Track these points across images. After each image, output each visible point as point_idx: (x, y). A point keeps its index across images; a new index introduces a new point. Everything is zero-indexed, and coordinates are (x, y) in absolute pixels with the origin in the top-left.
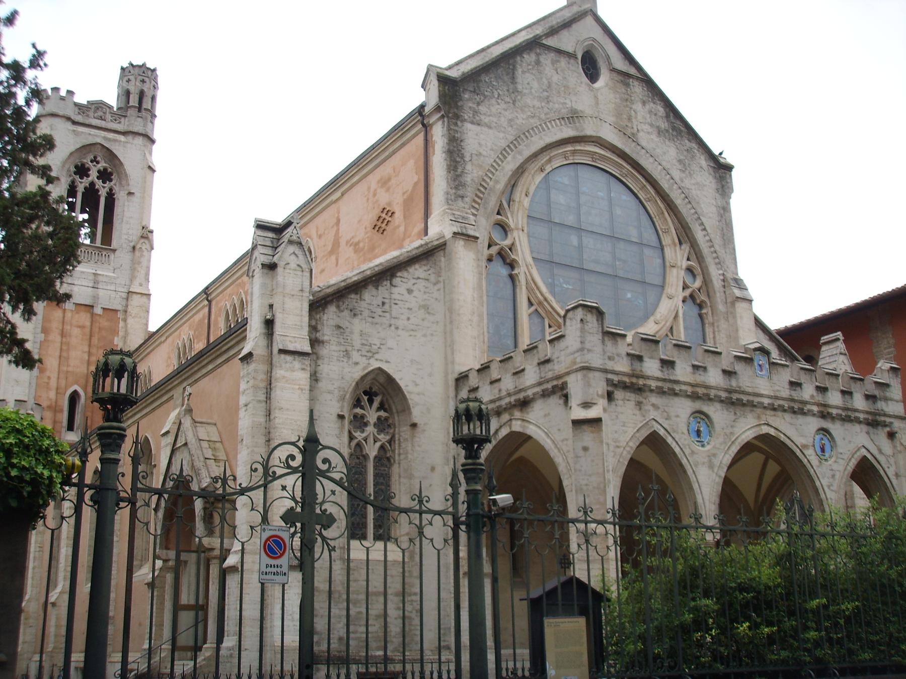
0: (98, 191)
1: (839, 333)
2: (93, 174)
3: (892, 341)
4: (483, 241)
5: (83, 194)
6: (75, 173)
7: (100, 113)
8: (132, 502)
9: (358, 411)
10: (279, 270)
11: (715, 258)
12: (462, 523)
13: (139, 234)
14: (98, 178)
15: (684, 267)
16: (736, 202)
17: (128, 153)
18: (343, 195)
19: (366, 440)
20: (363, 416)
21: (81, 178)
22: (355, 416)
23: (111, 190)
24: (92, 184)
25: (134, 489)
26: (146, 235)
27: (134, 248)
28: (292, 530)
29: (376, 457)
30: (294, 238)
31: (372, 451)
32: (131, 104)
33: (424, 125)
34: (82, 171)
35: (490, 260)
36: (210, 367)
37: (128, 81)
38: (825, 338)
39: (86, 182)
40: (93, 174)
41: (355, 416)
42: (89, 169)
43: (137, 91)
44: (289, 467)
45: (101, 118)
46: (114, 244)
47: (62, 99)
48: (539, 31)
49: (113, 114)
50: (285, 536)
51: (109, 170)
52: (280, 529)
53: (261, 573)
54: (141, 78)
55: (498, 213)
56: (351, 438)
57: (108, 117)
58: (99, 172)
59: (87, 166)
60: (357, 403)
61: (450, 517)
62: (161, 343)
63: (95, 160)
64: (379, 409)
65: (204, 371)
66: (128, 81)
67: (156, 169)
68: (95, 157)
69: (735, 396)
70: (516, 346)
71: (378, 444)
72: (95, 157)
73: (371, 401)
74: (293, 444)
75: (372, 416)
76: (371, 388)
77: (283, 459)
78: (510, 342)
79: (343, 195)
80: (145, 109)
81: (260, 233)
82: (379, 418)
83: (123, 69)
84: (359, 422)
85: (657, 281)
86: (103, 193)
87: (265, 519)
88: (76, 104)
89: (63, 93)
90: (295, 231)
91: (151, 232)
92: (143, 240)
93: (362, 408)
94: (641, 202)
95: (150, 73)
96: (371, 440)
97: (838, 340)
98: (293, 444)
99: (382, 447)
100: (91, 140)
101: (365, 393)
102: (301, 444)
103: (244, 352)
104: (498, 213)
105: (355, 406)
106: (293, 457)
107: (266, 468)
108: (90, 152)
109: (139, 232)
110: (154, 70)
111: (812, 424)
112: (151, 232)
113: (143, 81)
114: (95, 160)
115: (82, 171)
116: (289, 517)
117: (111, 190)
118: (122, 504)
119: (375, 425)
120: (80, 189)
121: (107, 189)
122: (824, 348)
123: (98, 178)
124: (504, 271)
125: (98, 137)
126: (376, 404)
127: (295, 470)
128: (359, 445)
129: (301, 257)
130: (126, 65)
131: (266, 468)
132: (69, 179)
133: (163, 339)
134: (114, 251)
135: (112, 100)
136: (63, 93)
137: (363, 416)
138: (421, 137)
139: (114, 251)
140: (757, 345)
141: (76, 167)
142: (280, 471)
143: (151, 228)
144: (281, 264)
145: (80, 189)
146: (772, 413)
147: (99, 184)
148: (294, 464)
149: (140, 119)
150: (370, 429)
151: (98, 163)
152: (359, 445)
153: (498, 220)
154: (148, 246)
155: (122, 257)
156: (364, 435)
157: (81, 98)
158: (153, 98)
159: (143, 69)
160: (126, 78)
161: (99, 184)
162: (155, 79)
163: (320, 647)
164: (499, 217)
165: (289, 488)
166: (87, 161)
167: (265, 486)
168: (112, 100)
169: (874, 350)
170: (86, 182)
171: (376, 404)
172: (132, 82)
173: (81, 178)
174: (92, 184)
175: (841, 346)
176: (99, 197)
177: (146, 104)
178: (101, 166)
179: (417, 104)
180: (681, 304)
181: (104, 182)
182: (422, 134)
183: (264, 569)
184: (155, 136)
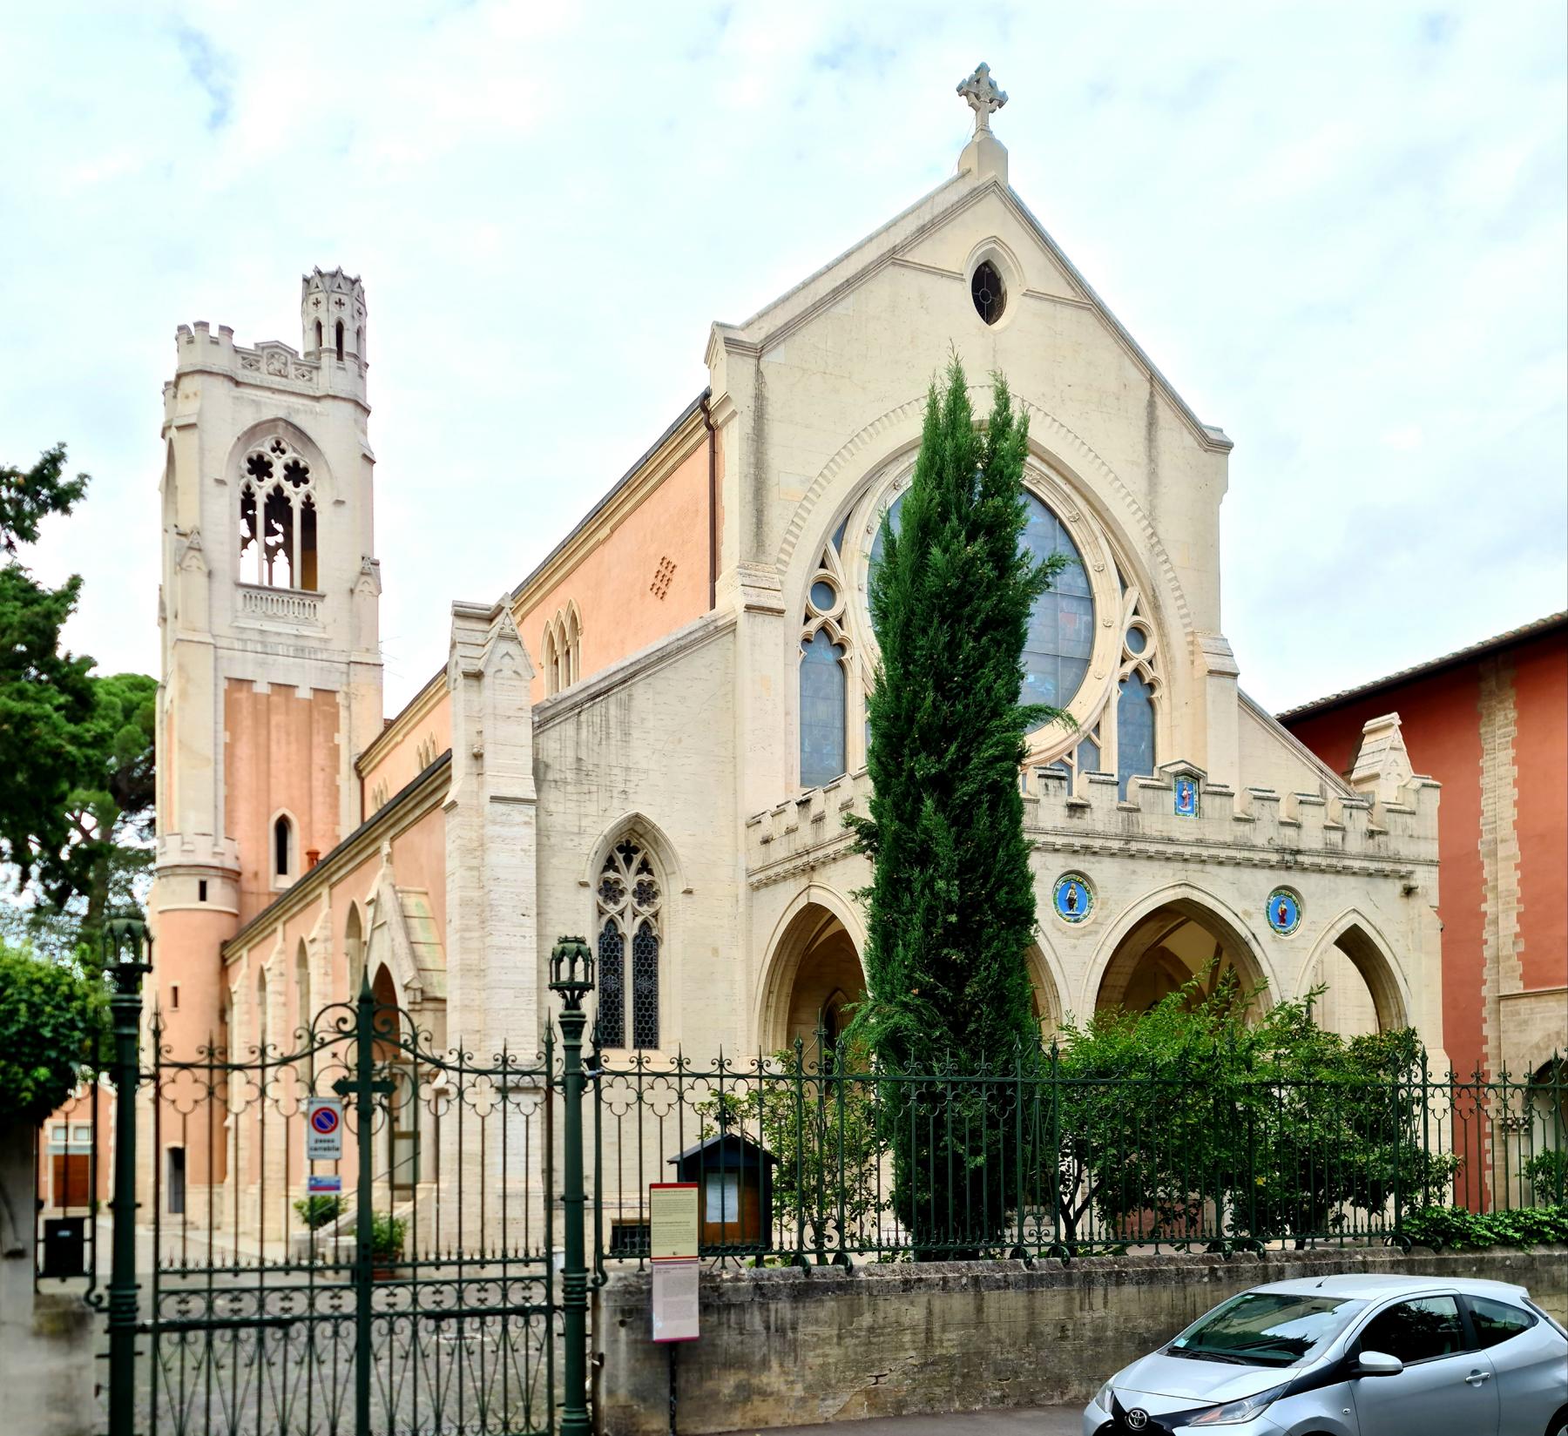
0: (288, 500)
1: (1395, 715)
2: (278, 471)
3: (1513, 715)
4: (795, 614)
5: (266, 505)
6: (251, 472)
7: (277, 365)
8: (155, 1077)
9: (611, 875)
10: (487, 680)
11: (1180, 608)
12: (558, 1084)
13: (358, 569)
14: (287, 478)
15: (1127, 626)
16: (1228, 509)
17: (326, 426)
18: (612, 532)
19: (621, 914)
20: (617, 882)
21: (260, 479)
22: (606, 882)
23: (308, 497)
24: (278, 489)
25: (158, 1065)
26: (370, 568)
27: (352, 591)
28: (345, 1101)
29: (636, 937)
30: (507, 630)
31: (629, 928)
32: (325, 345)
33: (710, 427)
34: (260, 467)
35: (807, 641)
36: (418, 812)
37: (317, 303)
38: (1370, 724)
39: (268, 485)
40: (278, 471)
41: (606, 882)
42: (270, 465)
43: (333, 323)
44: (340, 1031)
45: (280, 374)
46: (322, 586)
47: (215, 342)
48: (897, 237)
49: (299, 365)
50: (337, 1108)
51: (302, 464)
52: (331, 1101)
53: (311, 1149)
54: (336, 297)
55: (823, 565)
56: (601, 912)
57: (291, 370)
58: (287, 467)
59: (266, 459)
60: (610, 864)
61: (544, 1078)
62: (397, 744)
63: (277, 448)
64: (639, 872)
65: (411, 818)
66: (317, 303)
67: (376, 457)
68: (278, 443)
69: (1134, 846)
70: (844, 770)
71: (639, 920)
72: (278, 443)
73: (628, 861)
74: (344, 1005)
75: (629, 880)
76: (628, 842)
77: (333, 1023)
78: (835, 763)
79: (612, 532)
80: (349, 354)
81: (460, 623)
82: (640, 884)
83: (306, 281)
84: (610, 891)
85: (1079, 653)
86: (296, 505)
87: (312, 1089)
88: (236, 350)
89: (214, 331)
90: (507, 621)
91: (376, 564)
92: (364, 578)
93: (617, 870)
94: (1062, 524)
95: (346, 287)
96: (628, 914)
97: (1390, 726)
98: (344, 1005)
99: (645, 923)
100: (268, 414)
101: (620, 849)
102: (355, 1004)
103: (447, 801)
104: (823, 565)
105: (606, 869)
106: (344, 1021)
107: (312, 1037)
108: (269, 433)
109: (358, 565)
110: (355, 282)
111: (1266, 882)
112: (376, 564)
113: (340, 303)
114: (277, 448)
115: (260, 467)
116: (341, 1087)
117: (308, 497)
118: (143, 1081)
119: (634, 893)
120: (261, 500)
121: (302, 497)
122: (1366, 740)
123: (287, 478)
124: (830, 656)
125: (274, 406)
126: (635, 864)
127: (347, 1035)
128: (611, 921)
129: (519, 659)
130: (310, 274)
131: (312, 1037)
132: (243, 482)
133: (399, 738)
134: (323, 597)
135: (297, 339)
136: (214, 331)
137: (617, 882)
138: (705, 449)
139: (323, 597)
140: (1182, 767)
141: (250, 461)
142: (328, 1038)
143: (376, 557)
144: (489, 672)
145: (261, 500)
146: (1199, 867)
147: (288, 487)
148: (347, 1028)
149: (341, 373)
150: (628, 900)
151: (283, 452)
152: (611, 921)
153: (821, 577)
154: (372, 588)
155: (331, 610)
156: (618, 908)
157: (245, 339)
158: (359, 333)
159: (339, 280)
160: (312, 299)
161: (288, 487)
162: (360, 299)
163: (165, 1265)
164: (822, 571)
165: (341, 1056)
166: (265, 448)
167: (311, 1054)
168: (297, 339)
169: (1482, 730)
170: (268, 485)
171: (635, 864)
172: (323, 306)
173: (260, 479)
174: (278, 489)
175: (1394, 736)
176: (291, 509)
177: (349, 345)
178: (289, 457)
179: (697, 392)
180: (1116, 686)
181: (296, 485)
182: (707, 442)
183: (313, 1145)
184: (370, 401)
